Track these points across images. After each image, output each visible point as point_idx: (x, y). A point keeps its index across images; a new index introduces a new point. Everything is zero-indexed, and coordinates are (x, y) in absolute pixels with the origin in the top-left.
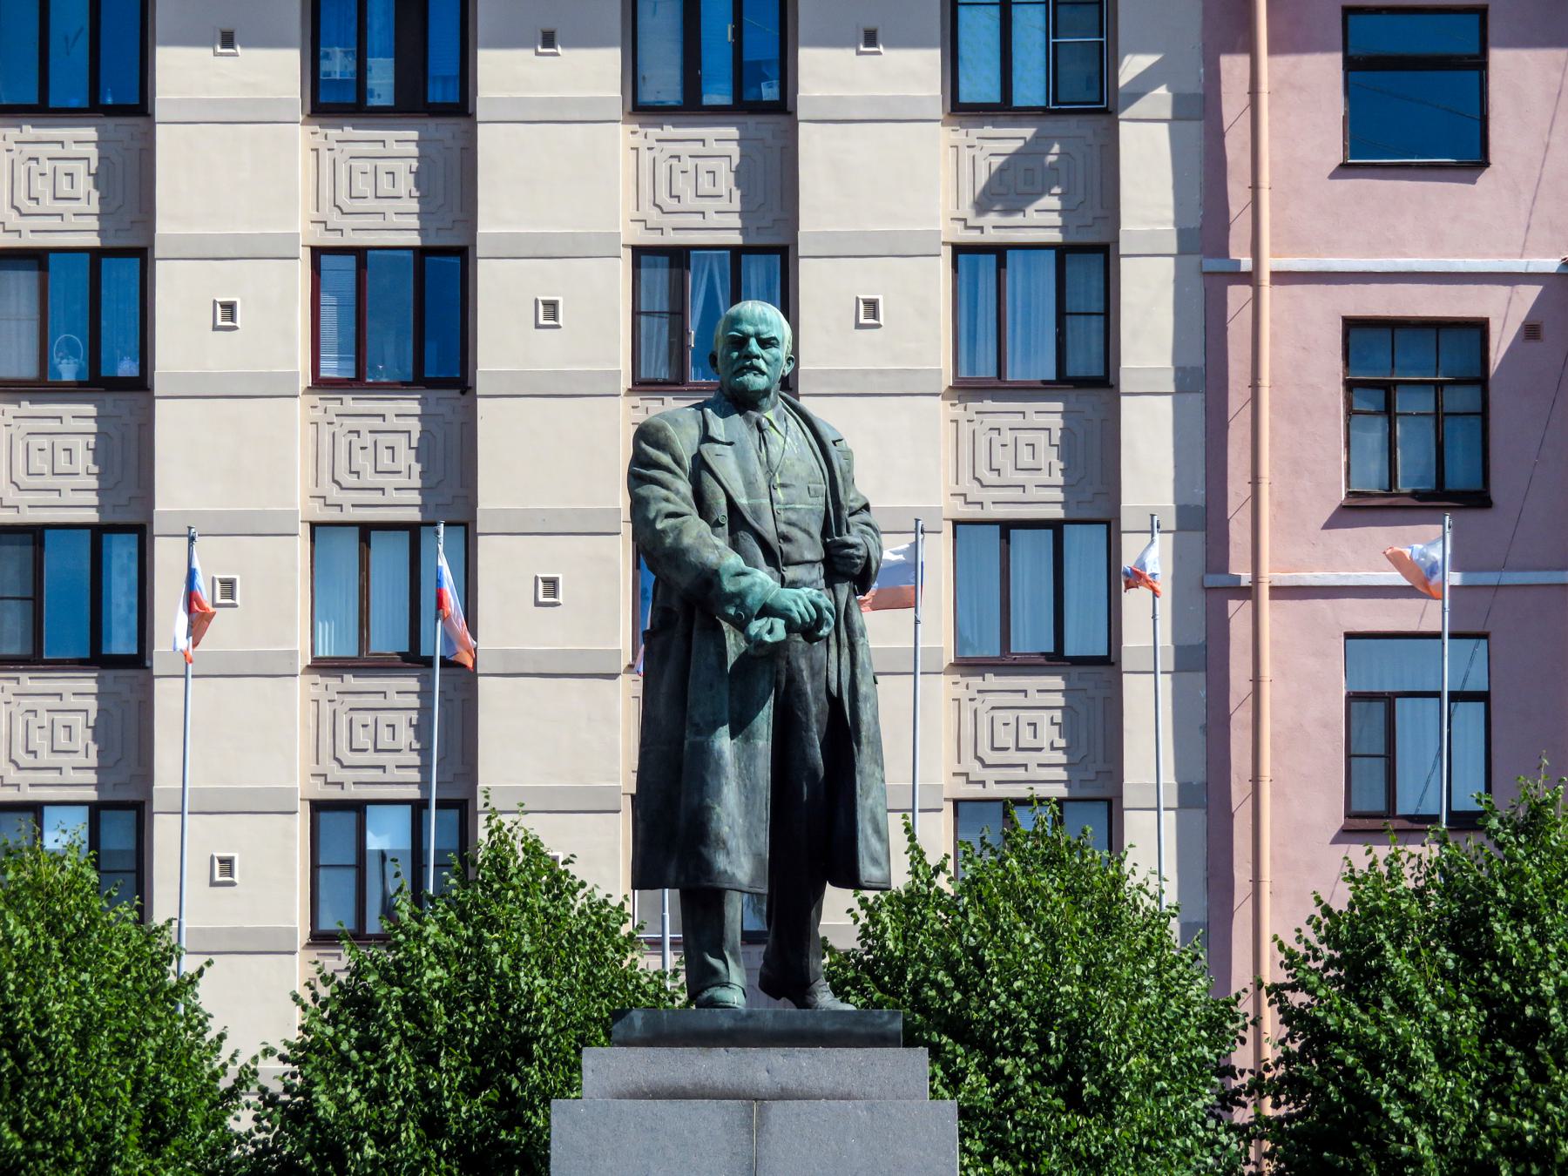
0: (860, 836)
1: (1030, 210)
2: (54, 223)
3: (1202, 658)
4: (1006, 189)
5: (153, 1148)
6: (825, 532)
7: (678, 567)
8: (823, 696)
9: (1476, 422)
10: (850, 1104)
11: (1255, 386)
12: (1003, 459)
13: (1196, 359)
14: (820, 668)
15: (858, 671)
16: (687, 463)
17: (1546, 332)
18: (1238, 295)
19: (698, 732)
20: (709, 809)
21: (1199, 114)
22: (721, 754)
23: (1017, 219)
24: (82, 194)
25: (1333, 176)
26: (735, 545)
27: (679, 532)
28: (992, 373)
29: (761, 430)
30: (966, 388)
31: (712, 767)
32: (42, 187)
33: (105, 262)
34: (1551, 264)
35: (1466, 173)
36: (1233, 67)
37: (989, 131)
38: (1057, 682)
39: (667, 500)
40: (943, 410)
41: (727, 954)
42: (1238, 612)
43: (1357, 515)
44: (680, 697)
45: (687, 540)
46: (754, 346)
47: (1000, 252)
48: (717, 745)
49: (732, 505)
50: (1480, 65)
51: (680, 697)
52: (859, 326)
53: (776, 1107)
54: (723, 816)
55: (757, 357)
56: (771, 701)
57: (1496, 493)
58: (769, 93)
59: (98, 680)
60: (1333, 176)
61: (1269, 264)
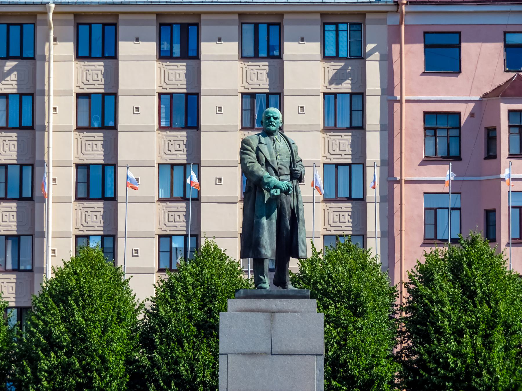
1: (343, 84)
2: (93, 86)
3: (387, 199)
6: (290, 167)
8: (290, 209)
10: (296, 314)
11: (401, 129)
12: (336, 147)
14: (288, 202)
16: (255, 149)
17: (476, 115)
18: (396, 106)
19: (258, 218)
21: (387, 61)
22: (263, 224)
24: (100, 79)
25: (421, 75)
26: (267, 170)
27: (253, 167)
28: (333, 125)
29: (274, 141)
32: (89, 77)
33: (106, 97)
36: (395, 47)
37: (333, 63)
38: (350, 205)
39: (250, 159)
40: (321, 135)
42: (396, 187)
45: (255, 169)
46: (272, 119)
47: (335, 94)
49: (266, 160)
50: (459, 47)
52: (299, 113)
53: (277, 315)
58: (276, 53)
59: (103, 204)
60: (421, 75)
61: (405, 98)
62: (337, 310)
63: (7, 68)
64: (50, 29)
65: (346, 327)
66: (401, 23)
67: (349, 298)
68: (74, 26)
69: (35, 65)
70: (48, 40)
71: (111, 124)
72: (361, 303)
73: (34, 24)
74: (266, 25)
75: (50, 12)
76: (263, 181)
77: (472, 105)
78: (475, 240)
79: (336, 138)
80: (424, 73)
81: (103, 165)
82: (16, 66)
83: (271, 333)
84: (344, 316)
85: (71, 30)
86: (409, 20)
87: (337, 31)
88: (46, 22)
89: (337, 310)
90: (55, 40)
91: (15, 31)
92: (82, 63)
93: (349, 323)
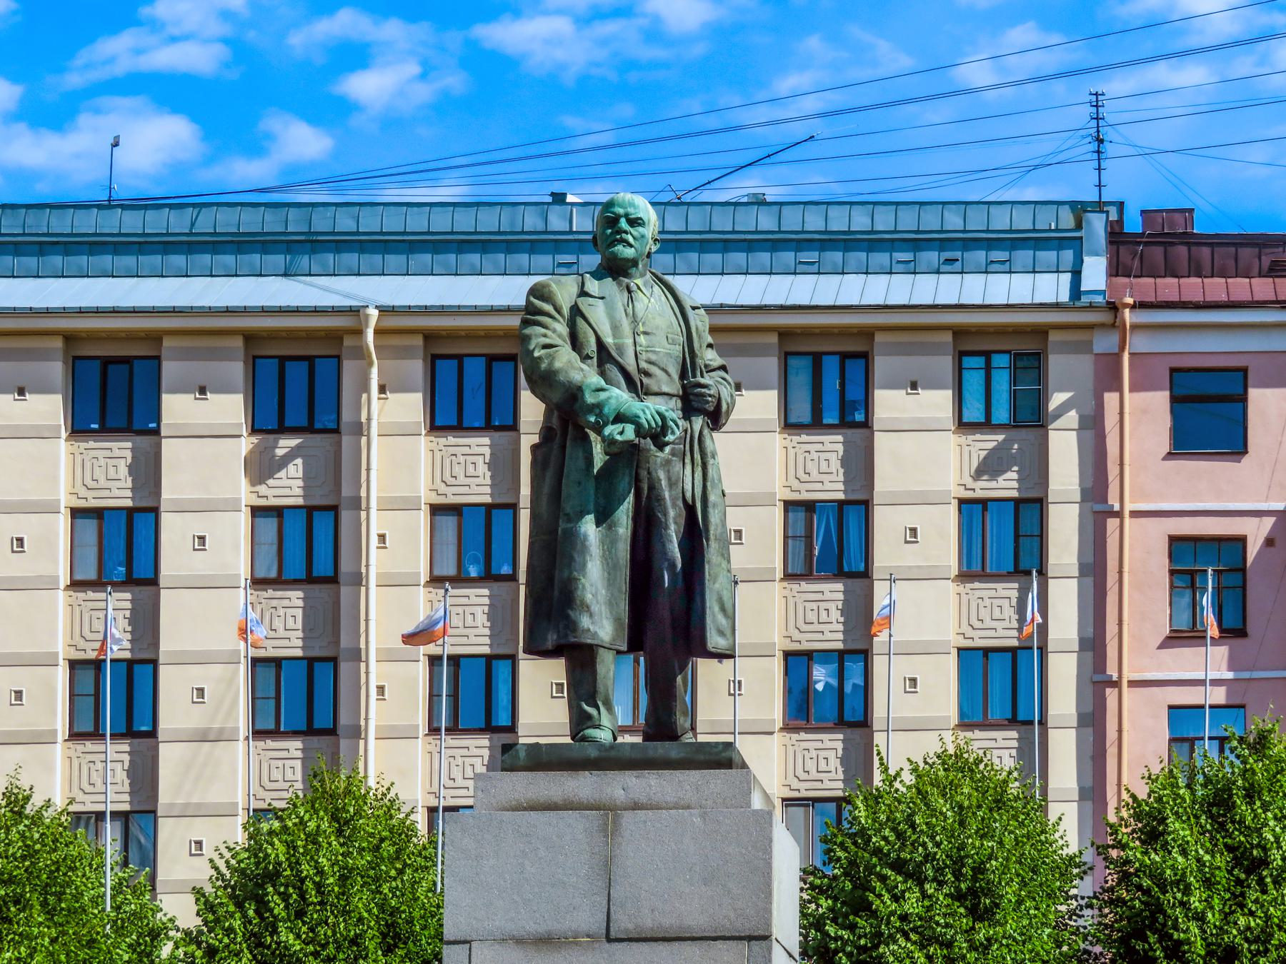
0: (708, 611)
1: (1000, 479)
2: (466, 490)
3: (1093, 720)
4: (990, 467)
5: (388, 951)
6: (683, 375)
7: (551, 386)
8: (680, 503)
9: (1239, 591)
10: (686, 813)
11: (1121, 572)
12: (984, 614)
13: (1090, 559)
14: (673, 478)
15: (709, 484)
16: (566, 311)
17: (1277, 543)
18: (1112, 523)
19: (569, 520)
20: (577, 580)
21: (1093, 426)
22: (586, 537)
23: (993, 484)
24: (481, 474)
25: (1164, 459)
26: (602, 374)
27: (552, 358)
28: (980, 568)
29: (630, 291)
30: (965, 576)
31: (579, 546)
32: (458, 470)
33: (494, 512)
34: (1279, 506)
35: (1234, 457)
36: (1111, 399)
37: (978, 437)
38: (1014, 734)
39: (545, 336)
40: (952, 587)
41: (600, 703)
42: (1111, 694)
43: (1174, 641)
44: (556, 495)
45: (558, 364)
46: (623, 224)
47: (984, 503)
48: (583, 530)
49: (601, 344)
50: (1243, 399)
51: (556, 495)
52: (907, 542)
53: (628, 818)
54: (587, 585)
55: (626, 232)
56: (631, 498)
57: (1249, 629)
58: (859, 417)
59: (490, 739)
60: (1164, 459)
61: (1128, 507)
62: (926, 903)
63: (280, 452)
64: (371, 364)
65: (949, 945)
66: (1122, 349)
67: (958, 875)
68: (424, 360)
69: (339, 444)
70: (366, 388)
71: (506, 570)
72: (988, 892)
73: (338, 357)
74: (837, 358)
75: (367, 326)
76: (584, 402)
77: (1269, 522)
78: (1265, 738)
79: (985, 594)
80: (1170, 456)
81: (489, 659)
82: (298, 447)
83: (607, 870)
84: (945, 915)
85: (417, 367)
86: (1139, 343)
87: (988, 369)
88: (361, 353)
89: (926, 903)
90: (382, 389)
91: (296, 373)
92: (443, 441)
93: (956, 933)
